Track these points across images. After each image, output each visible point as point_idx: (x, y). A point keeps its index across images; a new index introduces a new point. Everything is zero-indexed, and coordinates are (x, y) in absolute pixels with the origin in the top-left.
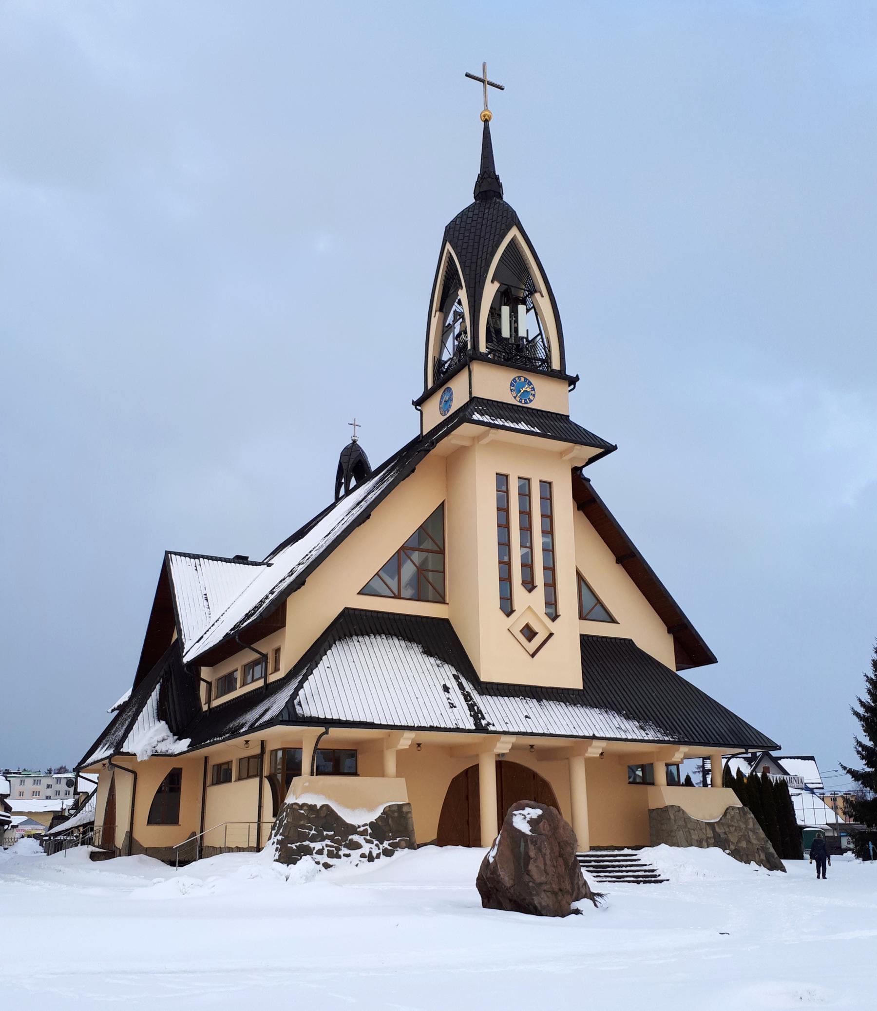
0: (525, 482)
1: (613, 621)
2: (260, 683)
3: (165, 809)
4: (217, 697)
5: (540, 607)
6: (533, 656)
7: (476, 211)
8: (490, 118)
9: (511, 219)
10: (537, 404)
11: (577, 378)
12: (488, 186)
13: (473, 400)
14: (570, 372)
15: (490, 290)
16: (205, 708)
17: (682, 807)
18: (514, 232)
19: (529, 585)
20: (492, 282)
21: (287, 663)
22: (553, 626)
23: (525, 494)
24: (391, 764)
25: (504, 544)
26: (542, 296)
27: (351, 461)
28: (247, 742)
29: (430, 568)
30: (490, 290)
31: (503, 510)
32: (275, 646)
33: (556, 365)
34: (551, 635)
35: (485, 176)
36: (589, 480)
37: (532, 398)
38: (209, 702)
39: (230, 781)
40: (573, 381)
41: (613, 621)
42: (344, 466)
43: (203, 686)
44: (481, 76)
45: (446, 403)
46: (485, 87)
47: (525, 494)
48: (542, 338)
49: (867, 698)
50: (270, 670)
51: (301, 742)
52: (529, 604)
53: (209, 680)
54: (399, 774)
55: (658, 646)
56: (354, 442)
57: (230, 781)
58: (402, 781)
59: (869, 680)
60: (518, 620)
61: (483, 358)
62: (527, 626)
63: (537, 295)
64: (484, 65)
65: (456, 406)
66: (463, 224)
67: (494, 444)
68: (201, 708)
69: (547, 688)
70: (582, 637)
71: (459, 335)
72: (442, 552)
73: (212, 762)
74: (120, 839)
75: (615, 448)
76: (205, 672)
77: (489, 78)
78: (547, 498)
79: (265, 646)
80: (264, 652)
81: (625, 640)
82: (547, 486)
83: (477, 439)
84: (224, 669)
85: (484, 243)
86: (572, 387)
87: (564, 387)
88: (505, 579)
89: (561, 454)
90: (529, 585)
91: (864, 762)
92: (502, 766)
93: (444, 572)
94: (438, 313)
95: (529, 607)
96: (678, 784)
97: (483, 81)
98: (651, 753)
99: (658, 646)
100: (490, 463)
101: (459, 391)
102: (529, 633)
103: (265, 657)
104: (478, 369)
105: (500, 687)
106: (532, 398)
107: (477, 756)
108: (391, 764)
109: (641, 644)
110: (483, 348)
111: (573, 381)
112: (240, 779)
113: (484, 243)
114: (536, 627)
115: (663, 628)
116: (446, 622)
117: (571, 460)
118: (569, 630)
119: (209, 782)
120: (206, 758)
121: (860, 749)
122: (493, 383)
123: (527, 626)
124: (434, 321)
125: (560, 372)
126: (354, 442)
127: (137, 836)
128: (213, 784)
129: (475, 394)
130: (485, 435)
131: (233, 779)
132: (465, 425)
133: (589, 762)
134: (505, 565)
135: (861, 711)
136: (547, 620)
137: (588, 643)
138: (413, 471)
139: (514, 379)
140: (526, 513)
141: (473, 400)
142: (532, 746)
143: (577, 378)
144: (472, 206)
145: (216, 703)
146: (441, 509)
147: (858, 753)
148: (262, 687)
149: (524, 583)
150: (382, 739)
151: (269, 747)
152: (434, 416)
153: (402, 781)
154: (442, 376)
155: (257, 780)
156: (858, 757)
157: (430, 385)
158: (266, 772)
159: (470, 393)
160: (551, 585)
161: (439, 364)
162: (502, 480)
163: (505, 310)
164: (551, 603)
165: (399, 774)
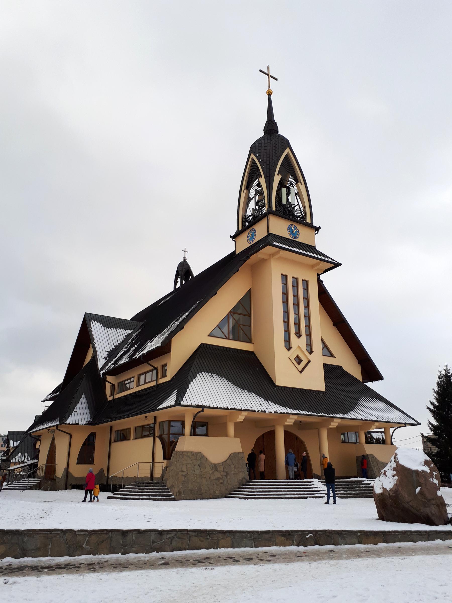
0: (296, 280)
1: (332, 356)
2: (154, 384)
3: (86, 454)
4: (118, 393)
5: (304, 348)
6: (301, 372)
7: (266, 140)
8: (271, 94)
9: (285, 143)
10: (300, 239)
11: (320, 228)
12: (271, 127)
13: (269, 234)
14: (316, 224)
15: (277, 179)
16: (110, 399)
17: (375, 455)
18: (287, 151)
19: (299, 335)
20: (278, 174)
21: (171, 374)
22: (310, 357)
23: (296, 286)
24: (231, 430)
25: (286, 312)
26: (302, 185)
27: (184, 270)
28: (146, 417)
29: (241, 323)
30: (277, 179)
31: (285, 294)
32: (163, 363)
33: (309, 221)
34: (309, 362)
35: (270, 122)
36: (323, 282)
37: (298, 236)
38: (112, 394)
39: (130, 439)
40: (317, 229)
41: (332, 356)
42: (180, 272)
43: (108, 386)
44: (267, 72)
45: (253, 237)
46: (269, 78)
47: (296, 286)
48: (299, 206)
49: (434, 401)
50: (159, 376)
51: (184, 417)
52: (298, 343)
53: (114, 383)
54: (235, 436)
55: (353, 369)
56: (185, 260)
57: (130, 439)
58: (238, 439)
59: (436, 392)
60: (293, 353)
61: (275, 214)
62: (298, 357)
63: (299, 184)
64: (268, 67)
65: (258, 238)
66: (260, 145)
67: (281, 258)
68: (107, 399)
69: (308, 390)
70: (324, 364)
71: (258, 202)
72: (250, 315)
73: (114, 429)
74: (60, 472)
75: (341, 264)
76: (109, 378)
77: (271, 74)
78: (306, 289)
79: (158, 363)
80: (156, 366)
81: (338, 366)
82: (306, 282)
83: (272, 255)
84: (123, 377)
85: (271, 157)
86: (317, 232)
87: (312, 232)
88: (287, 331)
89: (313, 266)
90: (299, 335)
91: (432, 432)
92: (287, 434)
93: (250, 326)
94: (245, 191)
95: (299, 346)
96: (372, 443)
97: (268, 75)
98: (357, 426)
99: (353, 369)
100: (277, 270)
101: (260, 231)
102: (299, 360)
103: (156, 368)
104: (273, 220)
105: (280, 388)
106: (298, 236)
107: (274, 426)
108: (231, 430)
109: (346, 368)
110: (274, 209)
111: (317, 229)
112: (135, 438)
113: (271, 157)
114: (302, 357)
115: (355, 361)
116: (251, 353)
117: (317, 270)
118: (318, 361)
119: (113, 440)
120: (111, 427)
121: (431, 426)
122: (279, 227)
123: (298, 357)
124: (243, 195)
125: (311, 224)
126: (185, 260)
127: (71, 470)
128: (115, 442)
129: (271, 232)
130: (278, 252)
131: (132, 437)
132: (268, 247)
133: (331, 432)
134: (287, 322)
135: (431, 407)
136: (307, 354)
137: (327, 367)
138: (238, 271)
139: (289, 226)
140: (296, 296)
141: (269, 234)
142: (301, 421)
143: (320, 228)
144: (262, 138)
145: (117, 396)
146: (248, 294)
147: (430, 428)
148: (154, 386)
149: (296, 333)
150: (226, 416)
151: (159, 420)
152: (244, 243)
153: (238, 439)
154: (246, 224)
155: (151, 439)
156: (429, 430)
157: (240, 228)
158: (157, 434)
159: (268, 231)
160: (309, 335)
161: (245, 217)
162: (285, 277)
163: (284, 190)
164: (309, 344)
165: (235, 436)
